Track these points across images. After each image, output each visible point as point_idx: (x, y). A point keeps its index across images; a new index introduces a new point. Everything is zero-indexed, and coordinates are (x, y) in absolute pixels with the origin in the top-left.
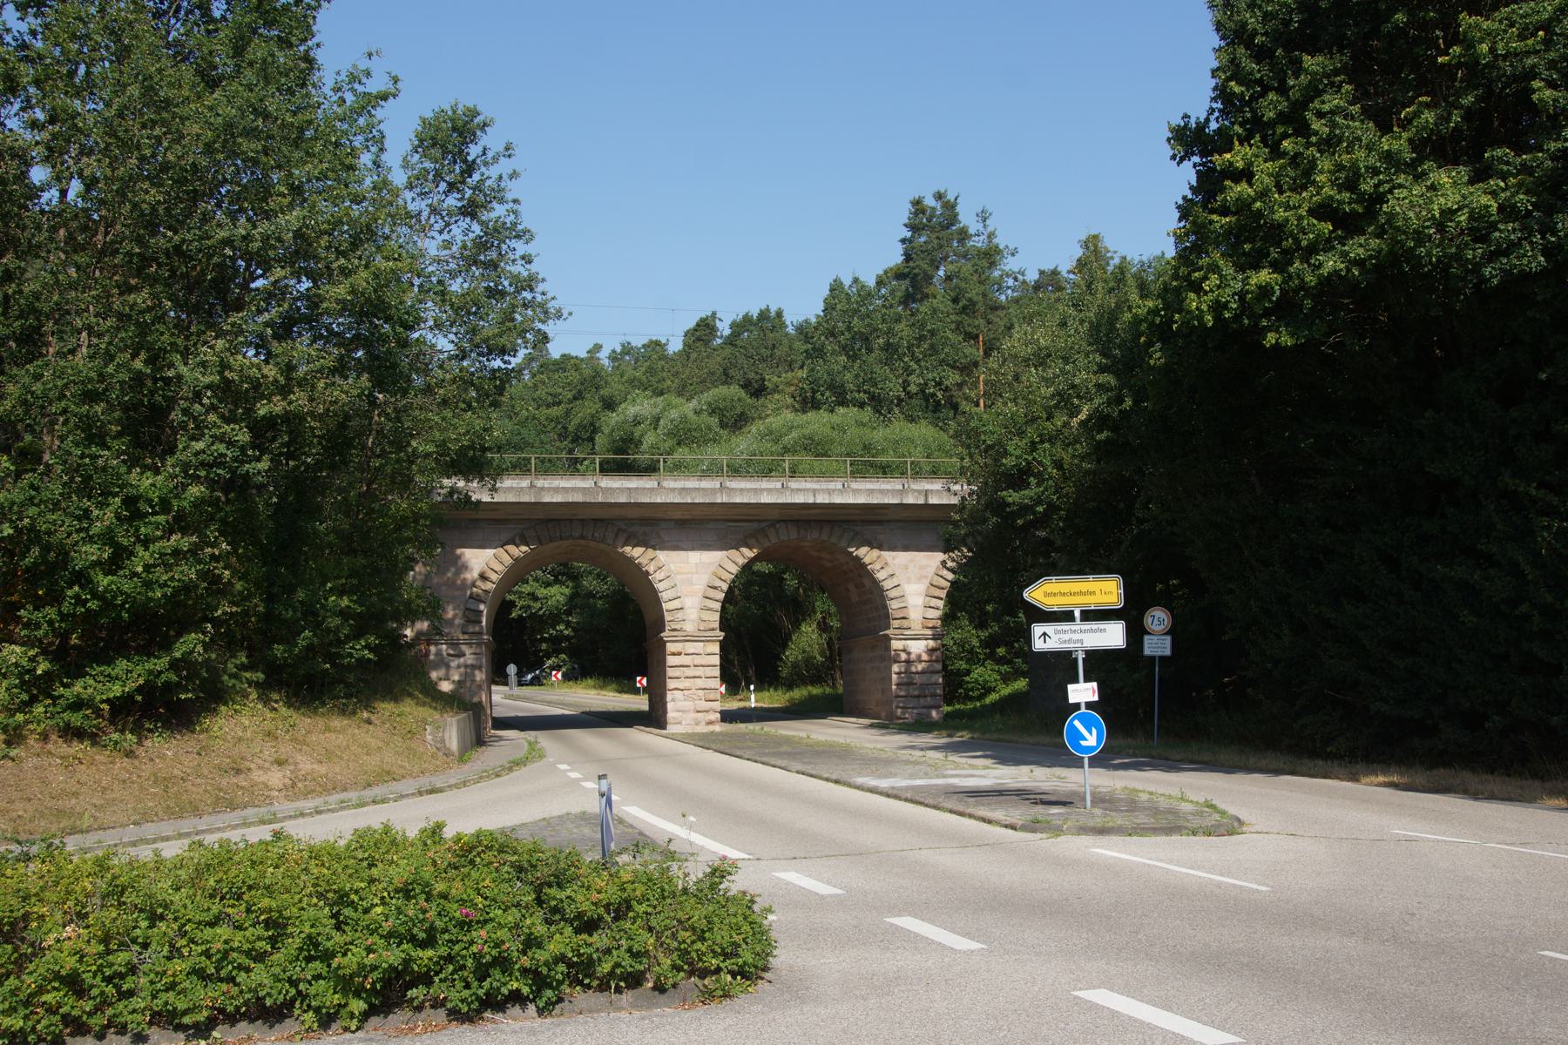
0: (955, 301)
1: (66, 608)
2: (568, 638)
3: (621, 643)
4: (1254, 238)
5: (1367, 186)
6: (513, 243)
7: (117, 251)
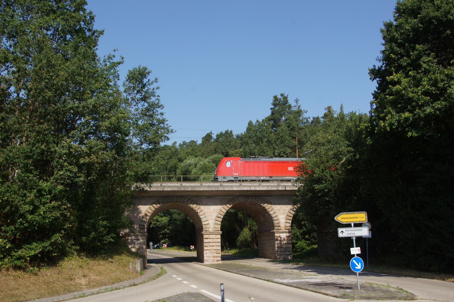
0: (289, 127)
1: (17, 226)
2: (168, 234)
3: (187, 235)
4: (402, 103)
5: (441, 85)
6: (158, 109)
7: (37, 111)
